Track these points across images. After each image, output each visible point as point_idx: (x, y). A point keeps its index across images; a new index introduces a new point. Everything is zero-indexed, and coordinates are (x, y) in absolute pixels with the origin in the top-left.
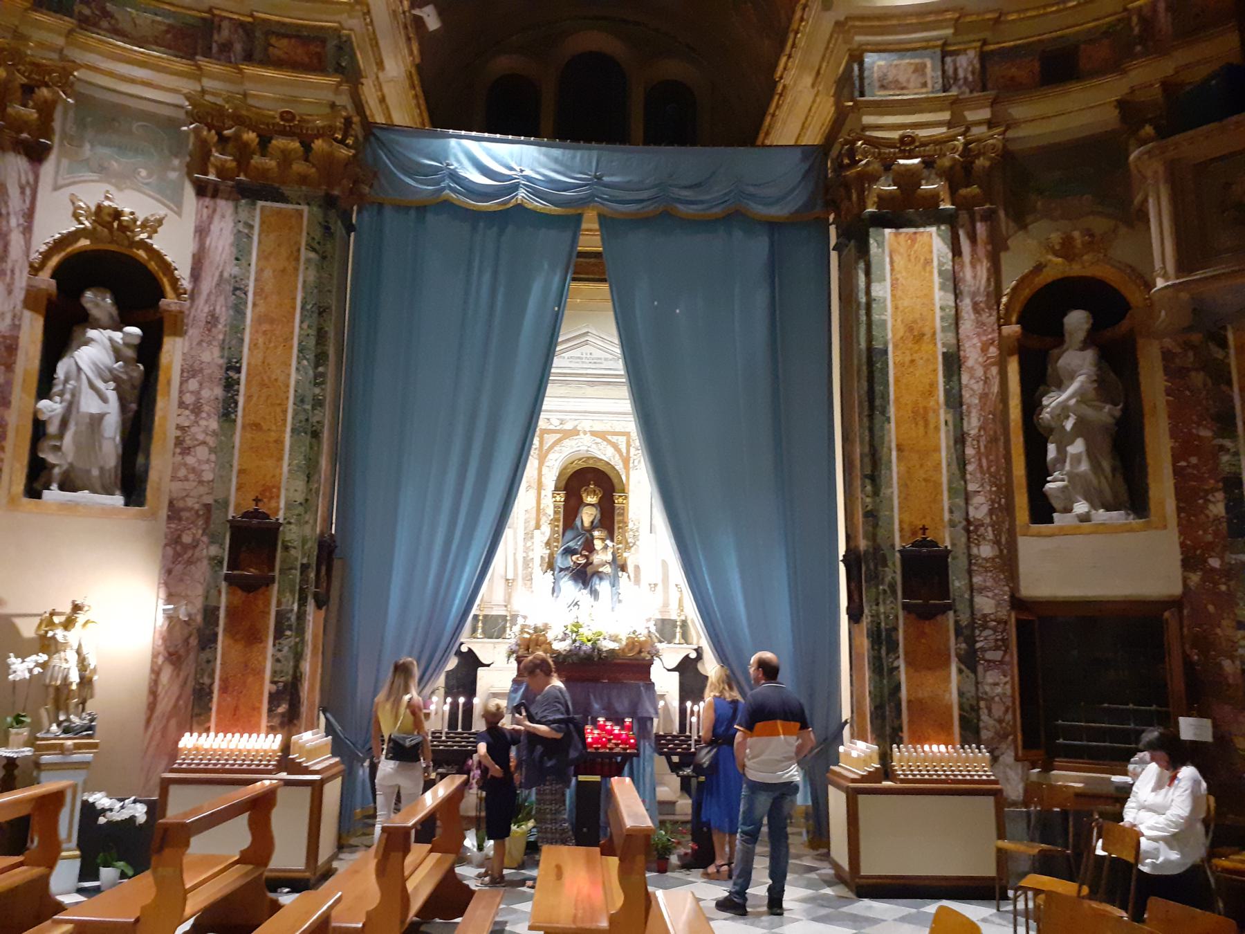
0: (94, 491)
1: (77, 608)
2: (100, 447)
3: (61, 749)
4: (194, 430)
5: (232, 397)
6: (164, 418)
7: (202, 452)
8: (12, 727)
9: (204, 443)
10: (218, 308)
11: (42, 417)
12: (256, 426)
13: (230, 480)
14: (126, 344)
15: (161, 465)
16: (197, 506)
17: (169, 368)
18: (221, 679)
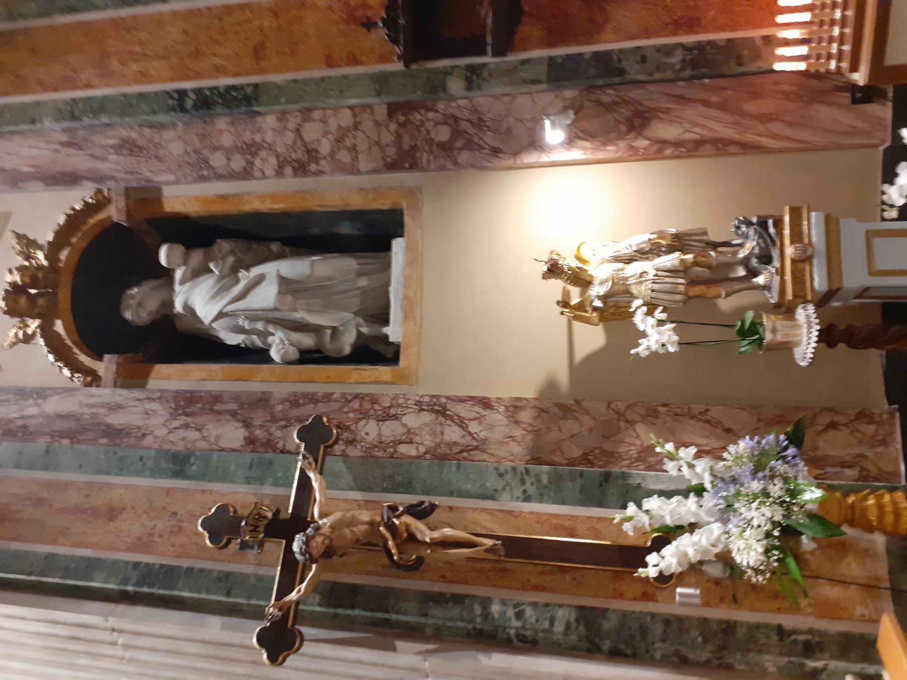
0: (388, 284)
1: (554, 270)
2: (329, 279)
3: (802, 261)
4: (280, 149)
5: (221, 95)
6: (273, 197)
7: (311, 132)
8: (761, 339)
9: (298, 131)
10: (110, 142)
11: (294, 354)
12: (258, 53)
13: (344, 77)
14: (185, 262)
15: (338, 191)
16: (393, 127)
17: (205, 200)
18: (675, 34)
